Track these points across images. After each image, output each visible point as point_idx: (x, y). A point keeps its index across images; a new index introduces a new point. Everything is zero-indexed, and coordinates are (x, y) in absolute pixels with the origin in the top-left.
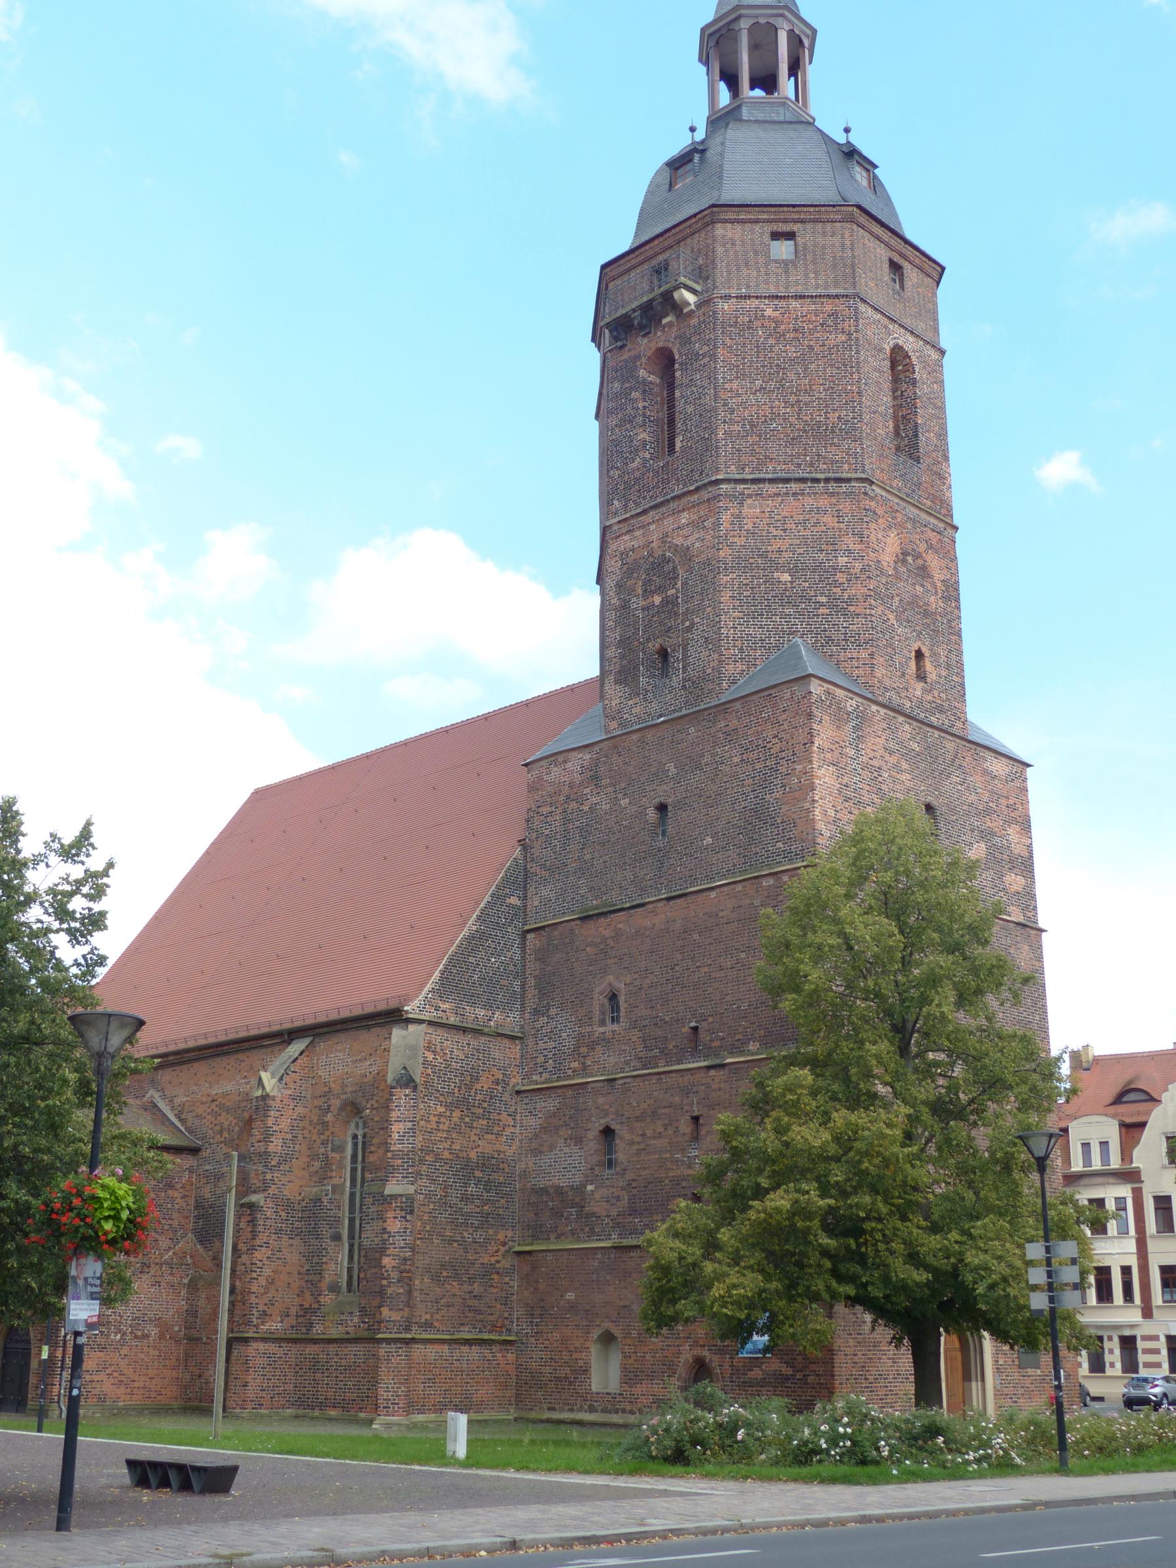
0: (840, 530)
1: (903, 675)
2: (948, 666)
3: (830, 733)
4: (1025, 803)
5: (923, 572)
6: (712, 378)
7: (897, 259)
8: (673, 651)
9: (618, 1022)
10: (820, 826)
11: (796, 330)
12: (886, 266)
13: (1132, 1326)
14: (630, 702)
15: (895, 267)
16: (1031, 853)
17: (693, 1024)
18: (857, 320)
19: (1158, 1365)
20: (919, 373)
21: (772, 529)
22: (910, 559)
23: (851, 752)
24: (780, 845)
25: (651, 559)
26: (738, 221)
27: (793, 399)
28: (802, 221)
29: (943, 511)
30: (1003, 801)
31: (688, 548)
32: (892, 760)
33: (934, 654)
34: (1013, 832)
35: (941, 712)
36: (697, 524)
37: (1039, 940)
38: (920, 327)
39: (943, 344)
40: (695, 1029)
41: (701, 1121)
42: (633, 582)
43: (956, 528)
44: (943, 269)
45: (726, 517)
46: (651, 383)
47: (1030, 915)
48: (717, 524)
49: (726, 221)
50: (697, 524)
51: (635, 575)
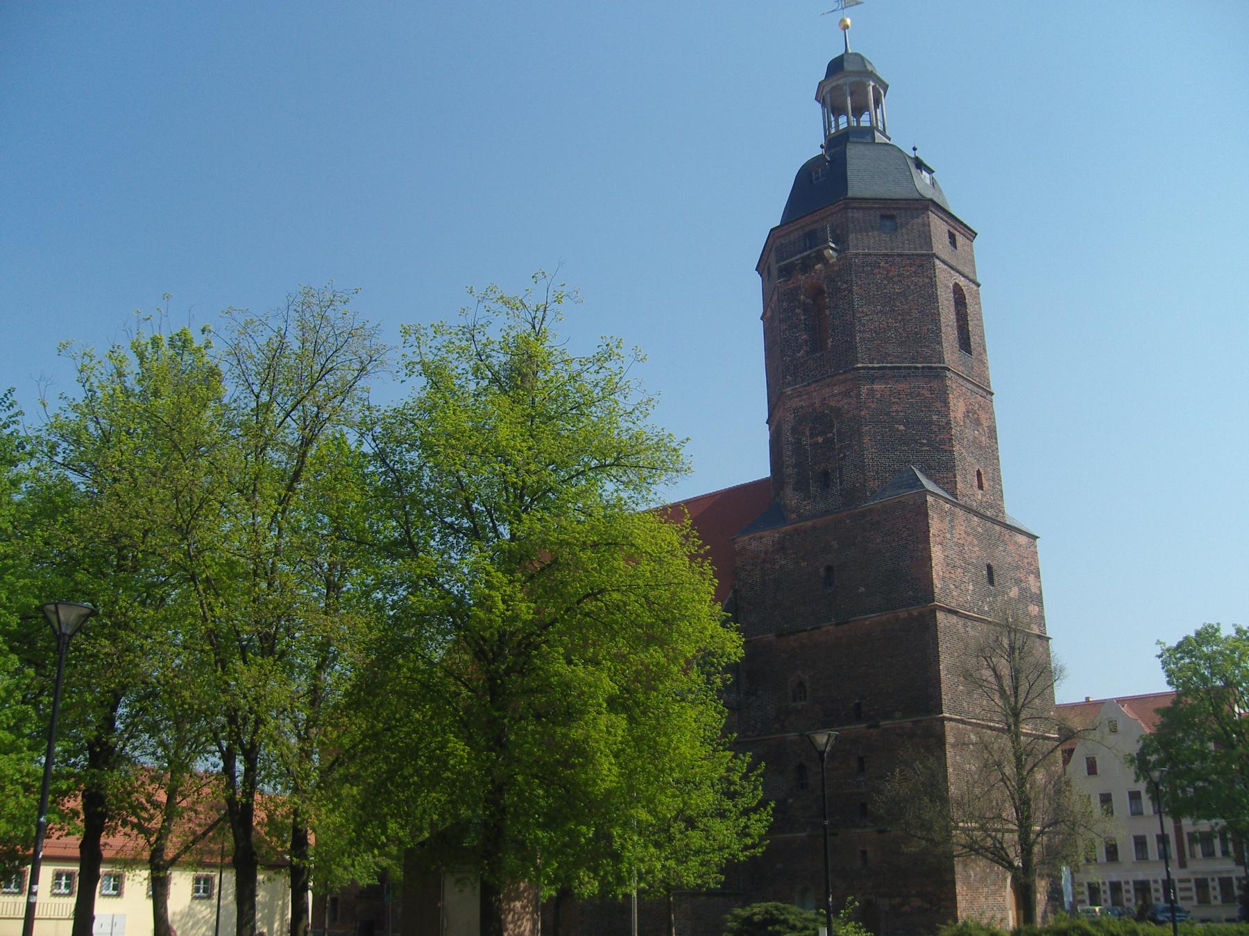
4: (1036, 561)
5: (978, 422)
10: (936, 581)
13: (1229, 871)
15: (952, 237)
19: (1191, 898)
23: (948, 536)
28: (899, 209)
32: (970, 539)
33: (986, 472)
34: (1031, 578)
36: (847, 394)
38: (966, 271)
39: (979, 280)
40: (858, 705)
45: (864, 390)
50: (847, 394)
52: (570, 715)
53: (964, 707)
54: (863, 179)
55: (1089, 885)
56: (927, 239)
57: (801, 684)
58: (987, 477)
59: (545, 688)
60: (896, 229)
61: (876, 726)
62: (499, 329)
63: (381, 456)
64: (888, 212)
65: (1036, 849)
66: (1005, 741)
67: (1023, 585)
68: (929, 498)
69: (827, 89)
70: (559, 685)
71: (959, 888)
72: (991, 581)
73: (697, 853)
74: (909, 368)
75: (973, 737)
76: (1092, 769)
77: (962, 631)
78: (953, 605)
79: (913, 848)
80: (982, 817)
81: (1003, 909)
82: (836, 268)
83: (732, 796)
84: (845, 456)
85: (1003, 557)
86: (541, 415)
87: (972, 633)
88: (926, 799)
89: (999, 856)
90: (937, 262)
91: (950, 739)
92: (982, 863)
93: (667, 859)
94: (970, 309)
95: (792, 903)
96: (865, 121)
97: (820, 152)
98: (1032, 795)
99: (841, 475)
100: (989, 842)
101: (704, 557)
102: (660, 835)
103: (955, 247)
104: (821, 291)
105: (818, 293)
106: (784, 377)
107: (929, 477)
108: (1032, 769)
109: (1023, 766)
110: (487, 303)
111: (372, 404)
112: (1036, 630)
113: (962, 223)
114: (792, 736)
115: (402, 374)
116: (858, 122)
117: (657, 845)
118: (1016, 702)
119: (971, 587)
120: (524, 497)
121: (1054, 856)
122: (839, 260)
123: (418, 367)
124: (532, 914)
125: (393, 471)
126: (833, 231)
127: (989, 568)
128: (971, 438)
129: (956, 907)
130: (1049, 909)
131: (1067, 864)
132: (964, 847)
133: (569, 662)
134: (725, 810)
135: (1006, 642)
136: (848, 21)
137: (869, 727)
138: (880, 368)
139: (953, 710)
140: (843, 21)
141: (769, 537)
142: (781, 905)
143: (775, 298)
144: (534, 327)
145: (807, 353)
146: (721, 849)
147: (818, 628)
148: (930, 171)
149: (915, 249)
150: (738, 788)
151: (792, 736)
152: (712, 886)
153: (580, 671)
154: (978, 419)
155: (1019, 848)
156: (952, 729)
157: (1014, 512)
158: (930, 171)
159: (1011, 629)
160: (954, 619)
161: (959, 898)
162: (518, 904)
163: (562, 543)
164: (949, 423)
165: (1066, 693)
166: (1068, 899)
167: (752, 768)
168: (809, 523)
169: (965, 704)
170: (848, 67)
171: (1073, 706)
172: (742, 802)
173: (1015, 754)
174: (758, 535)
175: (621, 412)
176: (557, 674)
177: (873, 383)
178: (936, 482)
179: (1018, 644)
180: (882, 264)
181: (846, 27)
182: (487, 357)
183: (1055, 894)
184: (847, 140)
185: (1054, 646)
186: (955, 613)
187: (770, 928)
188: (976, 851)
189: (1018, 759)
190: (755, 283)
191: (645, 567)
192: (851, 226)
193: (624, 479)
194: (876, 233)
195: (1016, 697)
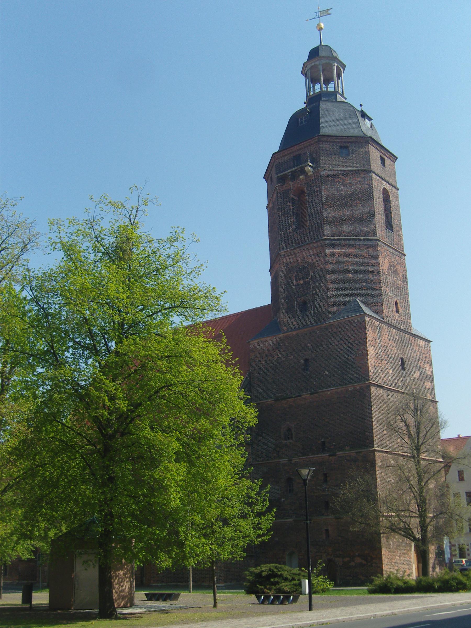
0: (369, 258)
1: (392, 311)
2: (405, 307)
3: (372, 335)
4: (430, 355)
5: (396, 272)
6: (321, 200)
7: (383, 156)
8: (309, 302)
9: (292, 439)
11: (350, 183)
12: (379, 159)
14: (292, 320)
15: (382, 160)
16: (432, 373)
17: (323, 440)
18: (372, 180)
20: (392, 198)
21: (345, 258)
22: (392, 268)
23: (378, 341)
24: (355, 375)
25: (298, 267)
26: (328, 142)
27: (350, 209)
28: (351, 142)
29: (401, 249)
30: (424, 355)
31: (313, 264)
32: (391, 343)
33: (401, 303)
34: (427, 366)
35: (404, 324)
36: (317, 255)
37: (437, 406)
38: (391, 180)
40: (324, 442)
41: (328, 475)
42: (291, 275)
43: (405, 255)
44: (397, 158)
45: (328, 253)
46: (295, 199)
47: (433, 396)
48: (325, 256)
49: (323, 141)
50: (317, 255)
51: (292, 272)
52: (154, 463)
53: (387, 444)
54: (329, 124)
55: (459, 545)
56: (367, 161)
57: (289, 430)
58: (401, 306)
59: (136, 443)
60: (349, 155)
61: (334, 455)
62: (109, 222)
63: (36, 300)
64: (344, 144)
65: (429, 528)
66: (411, 464)
67: (422, 370)
68: (367, 319)
69: (309, 67)
70: (146, 443)
71: (383, 552)
72: (403, 368)
73: (230, 540)
74: (355, 239)
75: (392, 462)
76: (461, 479)
77: (386, 398)
78: (380, 382)
79: (356, 529)
80: (398, 510)
81: (409, 563)
82: (312, 178)
83: (250, 505)
84: (316, 292)
85: (411, 353)
86: (134, 275)
87: (391, 399)
88: (365, 500)
89: (408, 533)
90: (373, 175)
91: (378, 463)
92: (397, 536)
93: (212, 544)
94: (393, 204)
95: (285, 564)
96: (331, 87)
97: (303, 106)
98: (428, 498)
99: (314, 302)
100: (402, 525)
101: (235, 365)
102: (207, 531)
103: (384, 166)
104: (303, 192)
105: (301, 193)
106: (280, 244)
107: (367, 305)
108: (427, 481)
109: (422, 480)
110: (101, 205)
111: (30, 268)
112: (430, 397)
113: (389, 152)
114: (284, 460)
115: (48, 250)
116: (327, 88)
117: (205, 536)
118: (418, 442)
119: (391, 372)
120: (123, 330)
121: (440, 532)
122: (314, 173)
123: (59, 245)
124: (130, 578)
125: (43, 309)
126: (311, 155)
127: (402, 360)
128: (392, 282)
129: (382, 563)
130: (436, 562)
131: (448, 536)
132: (387, 528)
133: (152, 428)
134: (246, 514)
135: (412, 406)
136: (322, 25)
137: (330, 456)
138: (338, 239)
139: (381, 445)
140: (319, 25)
141: (270, 341)
142: (278, 565)
143: (275, 196)
144: (130, 220)
145: (294, 229)
146: (243, 537)
147: (300, 396)
148: (370, 119)
149: (360, 167)
150: (254, 500)
151: (284, 460)
152: (238, 559)
153: (159, 435)
154: (396, 271)
155: (419, 528)
156: (380, 456)
157: (417, 326)
158: (370, 119)
159: (416, 398)
160: (381, 391)
161: (384, 557)
162: (121, 572)
163: (146, 356)
164: (379, 273)
165: (446, 434)
166: (447, 556)
167: (262, 488)
168: (294, 333)
169: (387, 442)
170: (321, 53)
171: (450, 441)
172: (256, 508)
173: (417, 473)
174: (264, 339)
175: (184, 273)
176: (145, 437)
177: (333, 248)
178: (370, 308)
179: (420, 407)
180: (340, 176)
181: (320, 29)
182: (102, 239)
183: (440, 553)
184: (321, 99)
185: (440, 406)
186: (382, 387)
187: (272, 580)
188: (394, 531)
189: (419, 476)
190: (262, 187)
191: (199, 371)
192: (322, 152)
193: (186, 314)
194: (337, 157)
195: (418, 439)
